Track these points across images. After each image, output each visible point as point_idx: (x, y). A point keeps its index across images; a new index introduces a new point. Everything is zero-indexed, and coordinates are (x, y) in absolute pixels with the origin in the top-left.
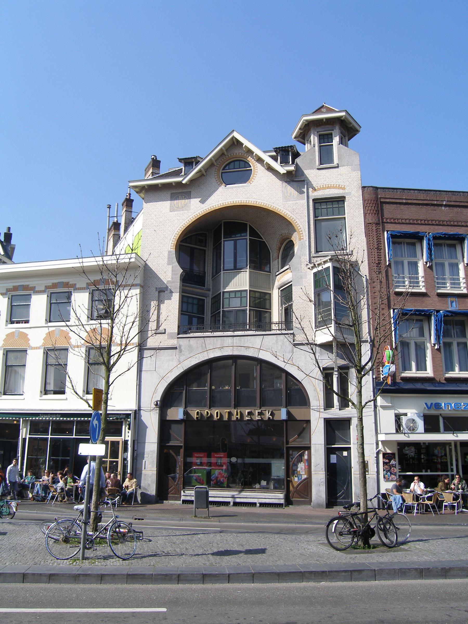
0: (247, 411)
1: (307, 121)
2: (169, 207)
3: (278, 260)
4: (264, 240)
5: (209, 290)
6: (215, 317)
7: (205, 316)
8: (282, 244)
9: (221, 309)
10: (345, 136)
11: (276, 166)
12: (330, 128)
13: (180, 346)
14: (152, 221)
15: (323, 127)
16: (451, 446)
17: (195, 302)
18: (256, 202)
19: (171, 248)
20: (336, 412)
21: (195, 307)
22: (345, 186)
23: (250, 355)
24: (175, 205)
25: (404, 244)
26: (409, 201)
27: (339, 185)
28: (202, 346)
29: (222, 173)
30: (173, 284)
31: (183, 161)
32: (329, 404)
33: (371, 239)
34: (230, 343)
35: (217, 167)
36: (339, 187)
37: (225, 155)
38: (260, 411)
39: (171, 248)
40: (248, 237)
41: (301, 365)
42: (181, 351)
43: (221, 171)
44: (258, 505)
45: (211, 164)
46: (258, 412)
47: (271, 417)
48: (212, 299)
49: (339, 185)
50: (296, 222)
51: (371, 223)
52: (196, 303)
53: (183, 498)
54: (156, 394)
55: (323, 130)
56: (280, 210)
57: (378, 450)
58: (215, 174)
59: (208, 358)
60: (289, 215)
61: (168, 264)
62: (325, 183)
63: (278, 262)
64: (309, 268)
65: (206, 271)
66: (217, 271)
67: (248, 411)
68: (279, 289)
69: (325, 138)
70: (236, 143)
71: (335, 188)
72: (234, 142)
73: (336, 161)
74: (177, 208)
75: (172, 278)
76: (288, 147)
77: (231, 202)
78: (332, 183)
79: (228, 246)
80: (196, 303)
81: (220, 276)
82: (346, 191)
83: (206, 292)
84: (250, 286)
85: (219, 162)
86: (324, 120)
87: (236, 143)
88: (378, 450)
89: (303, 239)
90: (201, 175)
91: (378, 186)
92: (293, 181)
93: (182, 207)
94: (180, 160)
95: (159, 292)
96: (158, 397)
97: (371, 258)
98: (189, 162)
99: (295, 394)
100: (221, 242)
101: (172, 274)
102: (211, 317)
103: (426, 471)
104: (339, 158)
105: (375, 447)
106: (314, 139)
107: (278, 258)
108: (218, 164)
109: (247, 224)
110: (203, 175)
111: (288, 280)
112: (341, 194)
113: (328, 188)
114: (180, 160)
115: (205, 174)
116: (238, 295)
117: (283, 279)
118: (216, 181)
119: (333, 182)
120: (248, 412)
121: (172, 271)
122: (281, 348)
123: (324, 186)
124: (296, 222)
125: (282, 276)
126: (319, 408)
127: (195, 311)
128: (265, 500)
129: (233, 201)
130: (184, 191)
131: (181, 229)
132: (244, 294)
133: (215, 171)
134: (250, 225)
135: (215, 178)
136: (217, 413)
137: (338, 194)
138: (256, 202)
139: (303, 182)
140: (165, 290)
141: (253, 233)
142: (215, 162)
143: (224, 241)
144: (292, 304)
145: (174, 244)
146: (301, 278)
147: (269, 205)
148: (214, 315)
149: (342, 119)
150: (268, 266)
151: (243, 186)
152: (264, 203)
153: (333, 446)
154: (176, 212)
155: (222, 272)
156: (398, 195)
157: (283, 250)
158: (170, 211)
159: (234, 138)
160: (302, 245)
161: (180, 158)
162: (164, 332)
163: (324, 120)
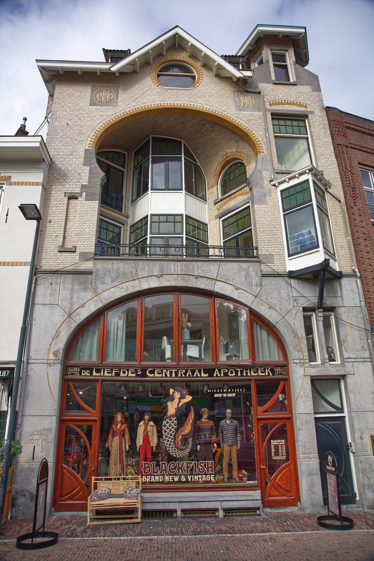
1: (262, 31)
2: (88, 100)
4: (199, 164)
9: (149, 236)
12: (284, 48)
14: (65, 113)
18: (203, 107)
19: (89, 147)
20: (320, 367)
22: (306, 104)
24: (97, 99)
27: (300, 103)
30: (91, 189)
33: (342, 161)
34: (173, 270)
37: (163, 56)
39: (89, 147)
41: (274, 301)
44: (221, 514)
48: (131, 227)
49: (300, 103)
51: (340, 145)
54: (58, 340)
56: (233, 119)
59: (140, 289)
60: (244, 126)
61: (84, 165)
64: (274, 185)
65: (124, 194)
68: (220, 218)
70: (177, 45)
71: (296, 104)
72: (175, 44)
75: (89, 182)
77: (171, 104)
82: (309, 110)
83: (124, 218)
89: (263, 152)
91: (342, 110)
92: (247, 92)
93: (107, 102)
95: (70, 198)
97: (345, 181)
100: (149, 158)
101: (90, 177)
109: (181, 142)
111: (236, 205)
114: (106, 52)
117: (227, 205)
118: (152, 80)
119: (292, 98)
121: (90, 173)
122: (246, 279)
124: (254, 134)
125: (226, 203)
126: (302, 361)
128: (231, 503)
129: (174, 104)
131: (104, 126)
138: (203, 107)
140: (78, 196)
145: (93, 142)
146: (265, 195)
147: (219, 112)
151: (186, 90)
152: (213, 110)
155: (150, 191)
156: (361, 123)
158: (90, 105)
160: (263, 159)
162: (73, 250)
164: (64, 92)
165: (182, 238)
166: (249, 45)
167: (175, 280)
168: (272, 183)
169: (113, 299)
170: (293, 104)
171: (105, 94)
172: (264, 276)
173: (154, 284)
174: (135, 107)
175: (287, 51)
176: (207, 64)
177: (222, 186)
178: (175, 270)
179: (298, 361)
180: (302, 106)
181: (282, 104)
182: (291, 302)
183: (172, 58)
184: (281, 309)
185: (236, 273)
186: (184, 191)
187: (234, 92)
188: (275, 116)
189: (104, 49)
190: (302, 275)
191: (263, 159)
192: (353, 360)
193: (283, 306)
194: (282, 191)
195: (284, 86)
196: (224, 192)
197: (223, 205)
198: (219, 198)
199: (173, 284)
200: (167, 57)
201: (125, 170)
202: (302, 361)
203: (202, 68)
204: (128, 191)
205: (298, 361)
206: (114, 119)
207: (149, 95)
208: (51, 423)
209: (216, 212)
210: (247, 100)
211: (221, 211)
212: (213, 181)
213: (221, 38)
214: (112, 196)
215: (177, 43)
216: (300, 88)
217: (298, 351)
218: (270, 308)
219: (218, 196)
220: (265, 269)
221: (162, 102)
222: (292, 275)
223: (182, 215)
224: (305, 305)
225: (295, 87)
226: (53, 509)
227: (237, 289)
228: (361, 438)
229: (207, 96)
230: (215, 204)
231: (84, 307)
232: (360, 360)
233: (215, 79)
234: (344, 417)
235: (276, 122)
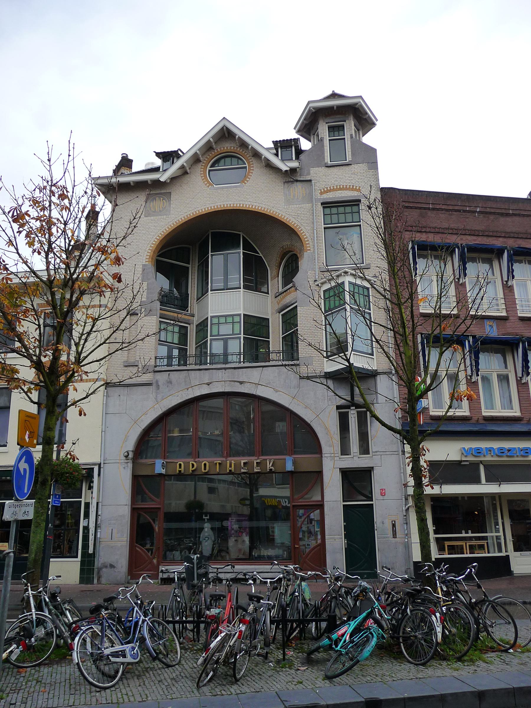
0: (242, 462)
3: (278, 279)
4: (261, 255)
5: (193, 316)
6: (201, 349)
7: (188, 348)
8: (282, 259)
9: (209, 338)
10: (358, 130)
11: (276, 162)
12: (342, 119)
13: (157, 382)
15: (332, 117)
16: (495, 500)
17: (177, 329)
20: (356, 461)
21: (176, 336)
23: (246, 392)
25: (431, 258)
26: (438, 207)
27: (353, 186)
28: (185, 382)
29: (210, 171)
31: (161, 156)
32: (345, 450)
34: (221, 378)
35: (203, 163)
36: (353, 189)
38: (258, 461)
39: (146, 262)
40: (241, 251)
42: (158, 387)
43: (208, 168)
45: (196, 160)
46: (257, 463)
47: (272, 468)
48: (197, 326)
49: (353, 186)
50: (302, 230)
52: (177, 331)
53: (161, 575)
55: (333, 120)
57: (407, 506)
58: (201, 171)
62: (336, 183)
63: (278, 281)
65: (189, 292)
66: (203, 292)
67: (245, 461)
68: (279, 313)
69: (336, 130)
70: (227, 135)
73: (349, 158)
74: (154, 212)
76: (291, 139)
78: (345, 184)
79: (216, 261)
80: (174, 360)
81: (208, 298)
84: (244, 309)
85: (206, 158)
86: (335, 108)
87: (227, 135)
88: (407, 506)
90: (184, 172)
92: (297, 181)
94: (158, 154)
96: (131, 445)
98: (168, 157)
99: (304, 437)
102: (196, 348)
103: (467, 532)
104: (353, 154)
105: (404, 503)
106: (323, 129)
107: (278, 277)
108: (205, 160)
110: (186, 173)
111: (291, 301)
112: (356, 196)
113: (340, 189)
114: (158, 154)
115: (188, 171)
116: (230, 320)
120: (244, 463)
123: (335, 187)
125: (284, 297)
126: (333, 455)
127: (176, 341)
130: (163, 192)
132: (237, 319)
133: (201, 168)
134: (244, 238)
135: (202, 177)
136: (205, 465)
137: (352, 196)
139: (309, 183)
141: (247, 246)
142: (200, 156)
143: (212, 255)
144: (297, 330)
145: (150, 256)
148: (199, 346)
149: (357, 106)
150: (266, 286)
153: (143, 486)
154: (152, 218)
155: (210, 292)
157: (285, 267)
159: (225, 128)
161: (157, 151)
163: (335, 108)
164: (122, 199)
165: (240, 338)
166: (305, 119)
167: (222, 386)
168: (316, 283)
169: (170, 406)
170: (346, 189)
171: (158, 204)
172: (301, 378)
173: (205, 390)
174: (186, 214)
175: (345, 121)
176: (256, 155)
177: (282, 277)
178: (222, 377)
179: (329, 455)
180: (356, 190)
181: (334, 190)
182: (326, 401)
183: (226, 147)
184: (316, 408)
185: (276, 377)
186: (242, 290)
187: (284, 183)
188: (326, 205)
189: (155, 152)
190: (336, 375)
191: (309, 257)
192: (381, 453)
193: (319, 408)
194: (325, 291)
195: (338, 168)
196: (285, 284)
197: (282, 299)
198: (280, 291)
199: (221, 390)
200: (217, 150)
201: (190, 266)
202: (333, 455)
203: (253, 158)
204: (193, 290)
205: (329, 455)
206: (167, 229)
207: (199, 198)
208: (125, 511)
209: (277, 307)
210: (298, 189)
211: (280, 305)
212: (275, 272)
213: (269, 124)
214: (175, 301)
215: (225, 133)
216: (355, 168)
217: (330, 446)
218: (306, 407)
219: (278, 289)
220: (304, 370)
221: (212, 205)
222: (329, 376)
223: (239, 315)
224: (339, 404)
225: (350, 167)
226: (129, 577)
227: (277, 391)
228: (383, 523)
229: (255, 194)
230: (276, 297)
231: (147, 414)
232: (388, 453)
233: (265, 171)
234: (373, 504)
235: (328, 211)
